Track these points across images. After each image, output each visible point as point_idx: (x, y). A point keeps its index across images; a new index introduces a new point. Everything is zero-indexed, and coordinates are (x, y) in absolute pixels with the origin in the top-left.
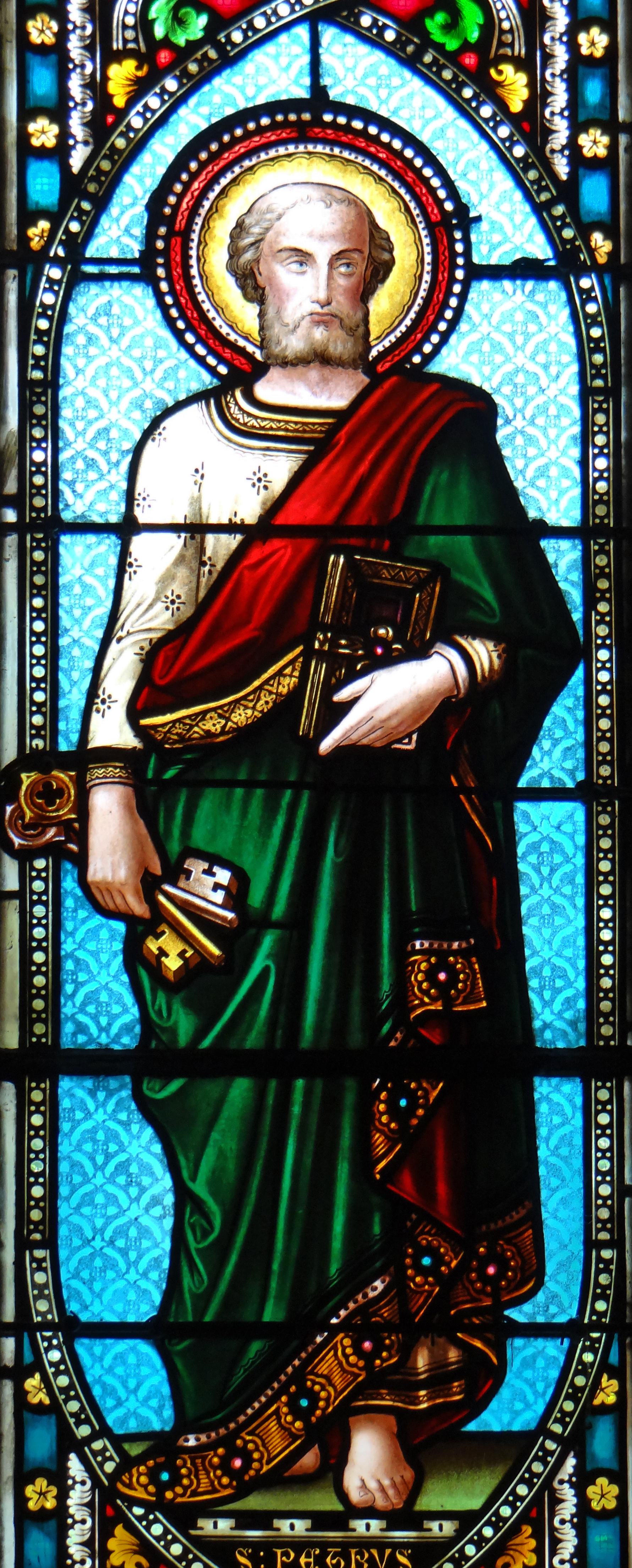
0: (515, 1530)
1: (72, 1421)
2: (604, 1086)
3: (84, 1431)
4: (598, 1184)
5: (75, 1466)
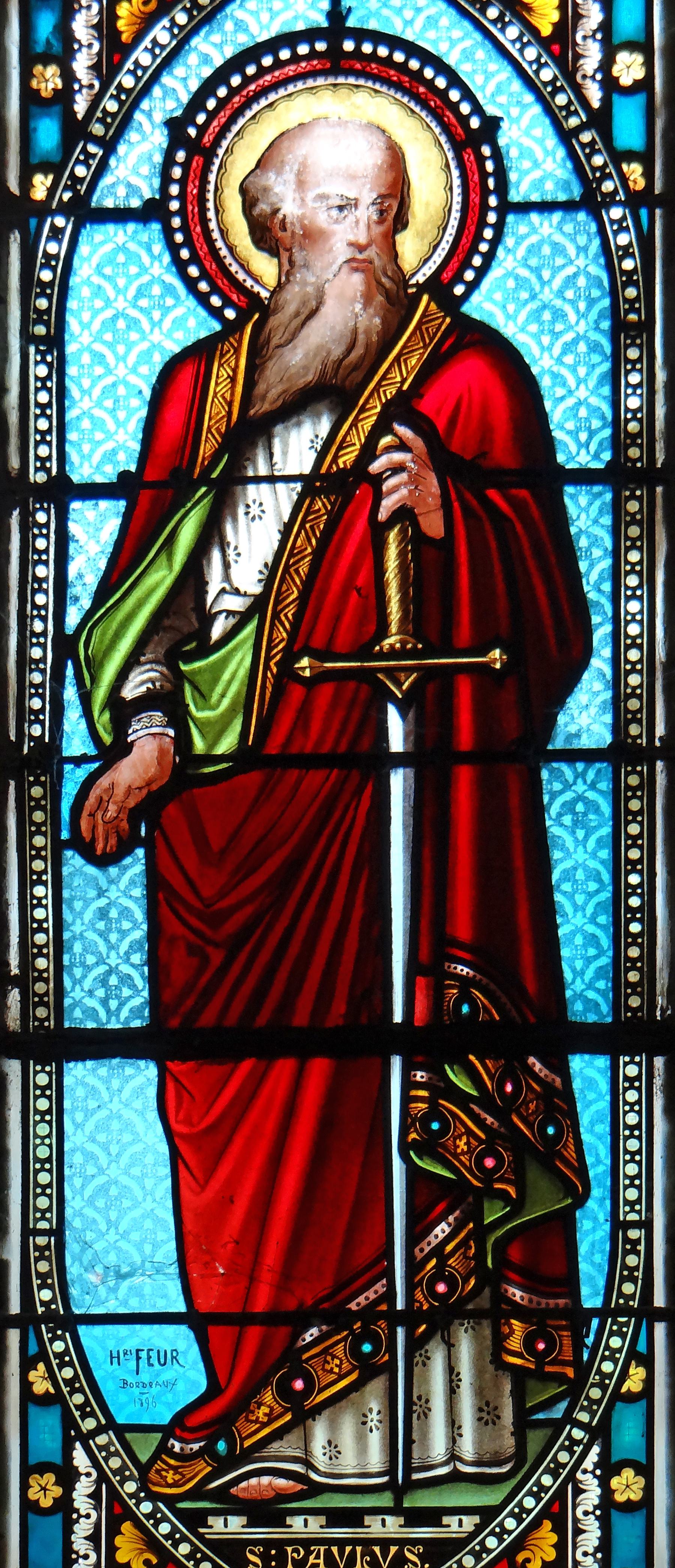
0: (536, 1524)
1: (77, 1414)
3: (89, 1424)
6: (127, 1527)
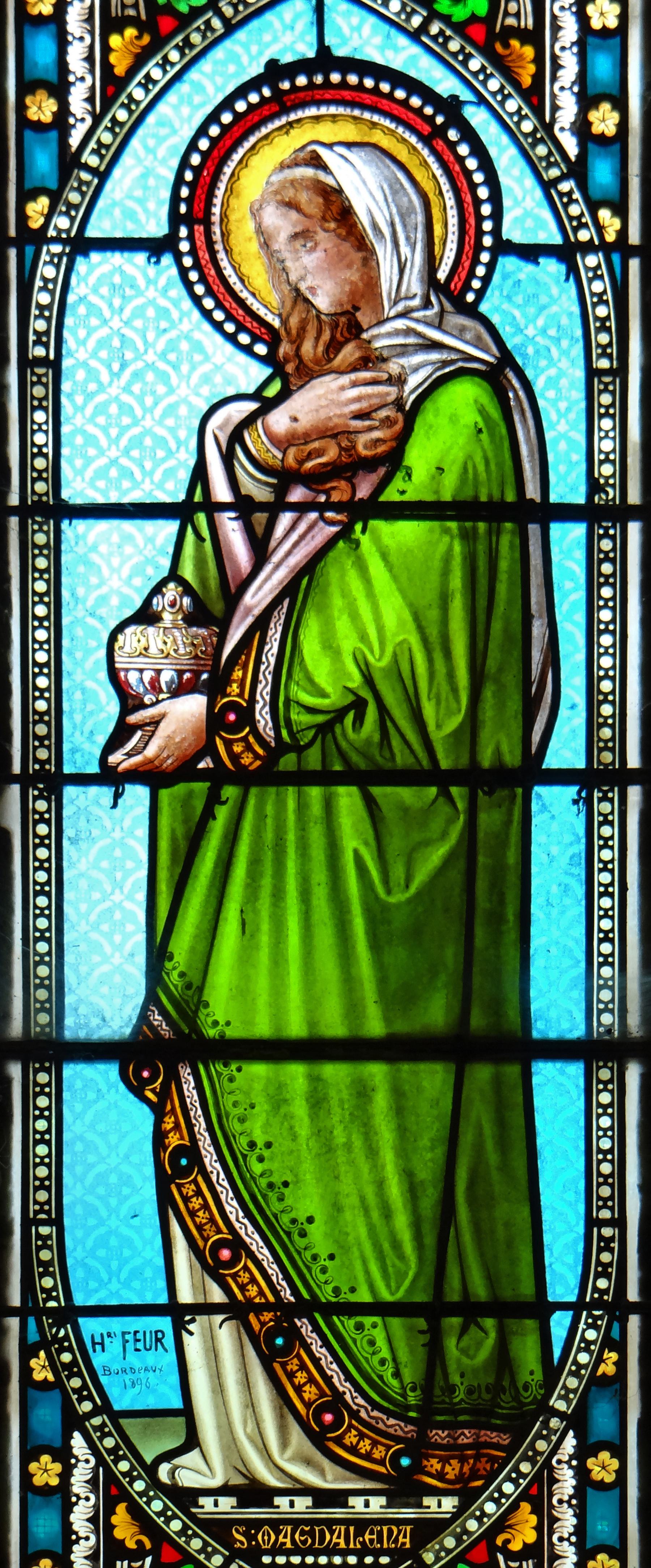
0: (514, 1507)
2: (605, 1066)
4: (599, 1162)
5: (78, 1442)
6: (121, 1508)
